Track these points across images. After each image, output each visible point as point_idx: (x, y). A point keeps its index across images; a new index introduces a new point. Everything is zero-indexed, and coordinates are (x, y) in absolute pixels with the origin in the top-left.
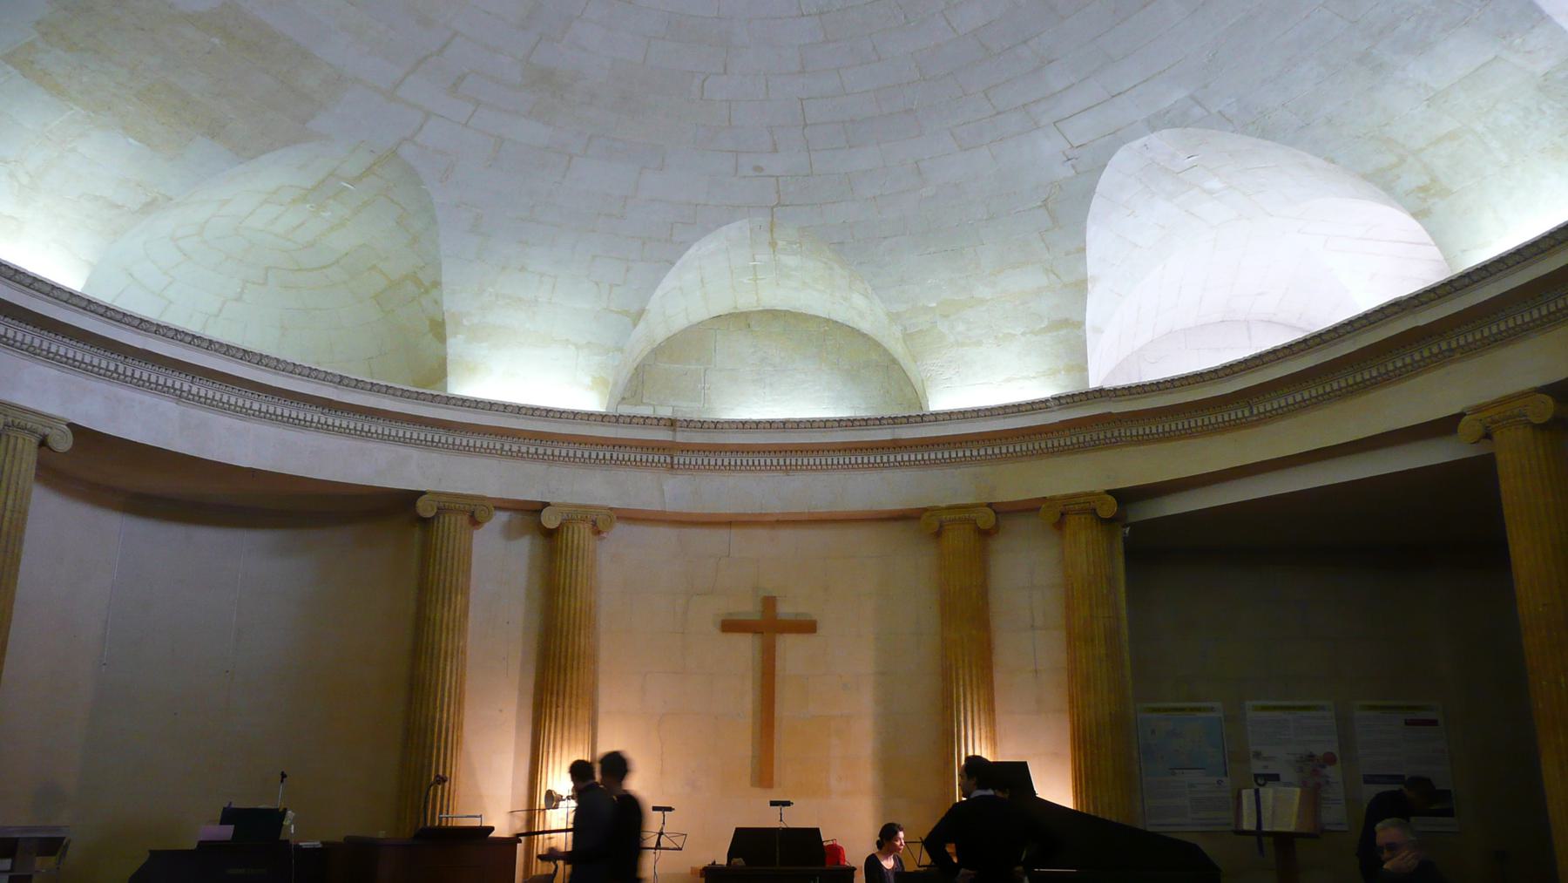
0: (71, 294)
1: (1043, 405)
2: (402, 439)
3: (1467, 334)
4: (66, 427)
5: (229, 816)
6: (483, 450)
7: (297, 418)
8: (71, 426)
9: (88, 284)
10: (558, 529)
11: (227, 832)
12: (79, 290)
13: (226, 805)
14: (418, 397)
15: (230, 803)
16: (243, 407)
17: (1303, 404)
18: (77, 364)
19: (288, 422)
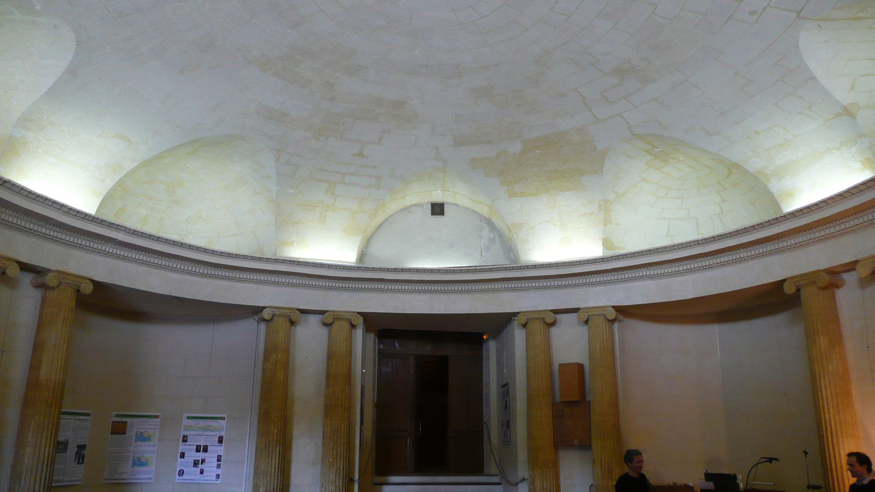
0: (86, 215)
1: (673, 248)
2: (401, 290)
3: (826, 230)
4: (611, 308)
5: (709, 477)
6: (398, 290)
7: (511, 287)
8: (613, 307)
9: (606, 243)
10: (555, 321)
11: (710, 485)
12: (94, 214)
13: (705, 472)
14: (513, 269)
15: (706, 471)
16: (305, 284)
17: (795, 246)
18: (182, 270)
19: (394, 291)
